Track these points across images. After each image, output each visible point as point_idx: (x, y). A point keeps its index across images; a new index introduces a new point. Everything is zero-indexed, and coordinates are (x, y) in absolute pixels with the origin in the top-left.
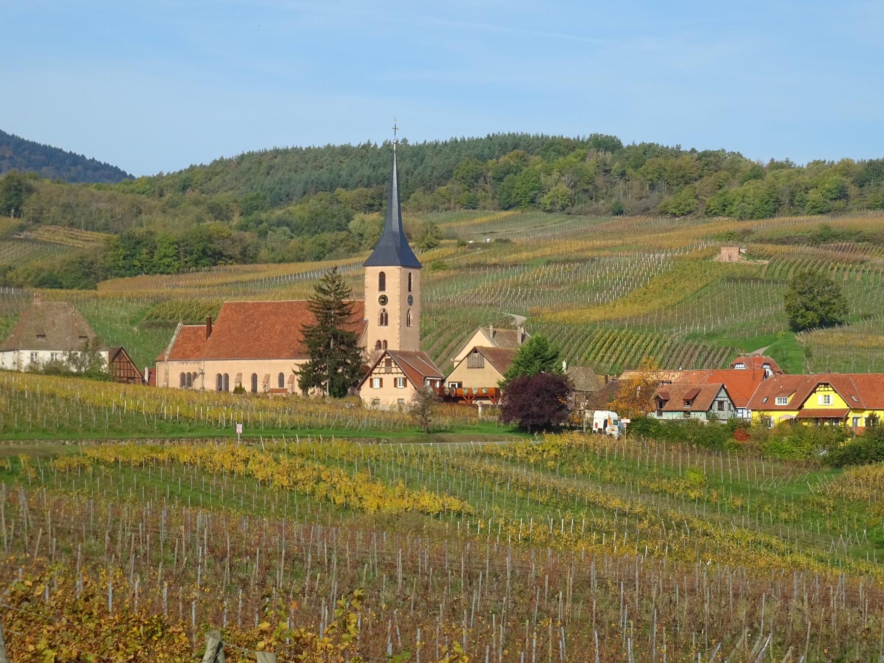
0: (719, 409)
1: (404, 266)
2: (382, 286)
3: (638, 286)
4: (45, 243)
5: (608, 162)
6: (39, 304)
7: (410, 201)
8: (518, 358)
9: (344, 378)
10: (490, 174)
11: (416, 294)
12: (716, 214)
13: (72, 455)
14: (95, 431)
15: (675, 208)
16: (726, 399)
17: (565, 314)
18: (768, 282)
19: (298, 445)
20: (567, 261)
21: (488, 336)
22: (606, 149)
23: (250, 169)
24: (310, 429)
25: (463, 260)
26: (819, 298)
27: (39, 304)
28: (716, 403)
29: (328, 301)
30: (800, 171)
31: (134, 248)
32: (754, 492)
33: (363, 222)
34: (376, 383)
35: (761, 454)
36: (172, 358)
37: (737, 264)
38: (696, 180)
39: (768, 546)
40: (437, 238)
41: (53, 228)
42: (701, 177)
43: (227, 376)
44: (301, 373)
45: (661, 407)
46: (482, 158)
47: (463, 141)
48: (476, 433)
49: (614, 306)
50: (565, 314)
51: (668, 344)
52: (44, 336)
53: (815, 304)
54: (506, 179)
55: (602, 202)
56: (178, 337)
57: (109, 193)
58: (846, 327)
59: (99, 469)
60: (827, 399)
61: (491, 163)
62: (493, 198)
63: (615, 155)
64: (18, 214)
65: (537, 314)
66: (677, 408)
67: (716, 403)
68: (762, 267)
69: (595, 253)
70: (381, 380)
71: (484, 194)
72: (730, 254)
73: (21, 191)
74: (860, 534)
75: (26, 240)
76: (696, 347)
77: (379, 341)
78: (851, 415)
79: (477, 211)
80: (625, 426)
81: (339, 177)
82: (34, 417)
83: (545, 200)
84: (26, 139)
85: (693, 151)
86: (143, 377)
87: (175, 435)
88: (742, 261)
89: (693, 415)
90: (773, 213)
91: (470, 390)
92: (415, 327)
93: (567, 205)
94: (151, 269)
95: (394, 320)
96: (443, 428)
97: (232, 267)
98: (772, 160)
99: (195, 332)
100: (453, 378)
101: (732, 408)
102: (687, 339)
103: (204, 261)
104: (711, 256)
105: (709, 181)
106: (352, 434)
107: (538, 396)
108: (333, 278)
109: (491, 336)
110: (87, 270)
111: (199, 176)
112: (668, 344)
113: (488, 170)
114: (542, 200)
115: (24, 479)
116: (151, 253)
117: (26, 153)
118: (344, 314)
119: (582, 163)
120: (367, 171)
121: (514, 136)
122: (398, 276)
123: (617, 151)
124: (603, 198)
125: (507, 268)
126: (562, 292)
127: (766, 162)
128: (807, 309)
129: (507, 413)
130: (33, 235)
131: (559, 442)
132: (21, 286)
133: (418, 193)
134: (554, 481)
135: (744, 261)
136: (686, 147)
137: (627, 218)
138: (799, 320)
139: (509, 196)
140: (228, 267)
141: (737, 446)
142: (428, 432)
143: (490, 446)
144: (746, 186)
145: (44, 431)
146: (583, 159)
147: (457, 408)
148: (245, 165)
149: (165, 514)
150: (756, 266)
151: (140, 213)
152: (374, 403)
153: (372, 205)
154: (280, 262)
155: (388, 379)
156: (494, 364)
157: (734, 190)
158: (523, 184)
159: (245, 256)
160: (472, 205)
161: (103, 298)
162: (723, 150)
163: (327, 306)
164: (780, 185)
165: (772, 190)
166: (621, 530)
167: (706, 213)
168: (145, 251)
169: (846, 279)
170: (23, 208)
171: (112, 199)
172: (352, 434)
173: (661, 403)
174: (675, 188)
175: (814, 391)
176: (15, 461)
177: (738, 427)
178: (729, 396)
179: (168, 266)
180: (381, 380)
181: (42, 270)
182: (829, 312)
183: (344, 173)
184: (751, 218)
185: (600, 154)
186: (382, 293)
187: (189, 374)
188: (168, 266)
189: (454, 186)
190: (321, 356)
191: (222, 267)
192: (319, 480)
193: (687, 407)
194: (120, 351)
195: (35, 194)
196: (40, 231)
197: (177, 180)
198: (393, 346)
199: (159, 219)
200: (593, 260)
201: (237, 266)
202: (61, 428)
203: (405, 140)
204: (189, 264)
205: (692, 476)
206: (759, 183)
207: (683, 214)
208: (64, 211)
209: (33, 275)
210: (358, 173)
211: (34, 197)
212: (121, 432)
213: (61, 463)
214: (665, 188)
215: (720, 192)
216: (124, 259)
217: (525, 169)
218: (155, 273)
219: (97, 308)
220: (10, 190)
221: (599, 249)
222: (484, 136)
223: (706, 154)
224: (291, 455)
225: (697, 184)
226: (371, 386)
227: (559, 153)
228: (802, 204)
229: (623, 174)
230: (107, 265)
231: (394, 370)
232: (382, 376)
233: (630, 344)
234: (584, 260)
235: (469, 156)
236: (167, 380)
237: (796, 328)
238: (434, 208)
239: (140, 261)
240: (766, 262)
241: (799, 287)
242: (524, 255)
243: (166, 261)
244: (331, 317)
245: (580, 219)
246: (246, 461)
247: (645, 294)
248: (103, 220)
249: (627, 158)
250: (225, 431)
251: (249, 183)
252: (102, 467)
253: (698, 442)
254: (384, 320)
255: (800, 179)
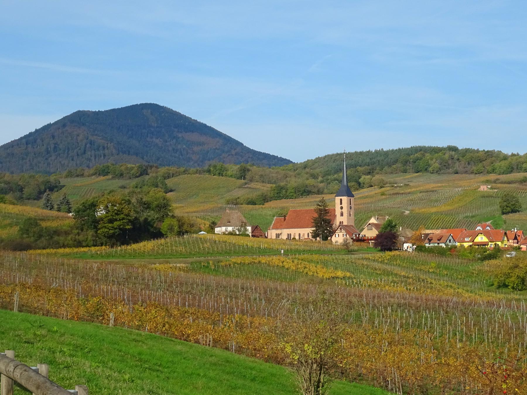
0: (449, 242)
1: (348, 196)
2: (341, 203)
3: (450, 200)
4: (253, 188)
5: (453, 155)
6: (228, 211)
7: (383, 170)
8: (383, 227)
9: (327, 234)
10: (411, 160)
11: (352, 206)
12: (491, 173)
13: (227, 261)
14: (237, 253)
15: (476, 171)
16: (452, 239)
17: (423, 210)
18: (496, 197)
19: (302, 256)
20: (427, 191)
21: (376, 219)
22: (453, 151)
23: (328, 160)
24: (310, 252)
25: (392, 192)
26: (511, 203)
27: (228, 211)
28: (448, 240)
29: (321, 209)
30: (521, 157)
31: (280, 190)
32: (452, 269)
33: (365, 179)
34: (337, 236)
35: (458, 257)
36: (273, 229)
37: (486, 191)
38: (484, 161)
39: (451, 287)
40: (384, 184)
41: (256, 183)
42: (486, 160)
43: (291, 234)
44: (312, 233)
45: (430, 242)
46: (409, 155)
47: (402, 149)
48: (366, 252)
49: (441, 207)
50: (423, 210)
51: (457, 220)
52: (230, 222)
53: (510, 205)
54: (417, 162)
55: (451, 169)
56: (275, 221)
57: (276, 171)
58: (521, 213)
59: (235, 265)
60: (482, 238)
61: (411, 156)
62: (412, 169)
63: (456, 153)
64: (244, 179)
65: (413, 210)
66: (435, 242)
67: (448, 240)
68: (494, 192)
69: (437, 189)
70: (339, 235)
71: (409, 167)
72: (484, 188)
73: (245, 170)
74: (483, 282)
75: (247, 188)
76: (467, 221)
77: (340, 222)
78: (490, 243)
79: (407, 174)
80: (414, 248)
81: (358, 163)
82: (218, 249)
83: (430, 169)
84: (257, 151)
85: (484, 150)
86: (265, 235)
87: (264, 254)
88: (488, 190)
89: (440, 245)
90: (511, 172)
91: (368, 237)
92: (352, 216)
93: (438, 171)
94: (287, 197)
95: (345, 214)
96: (353, 250)
97: (314, 196)
98: (512, 153)
99: (280, 220)
100: (362, 234)
101: (454, 242)
102: (464, 218)
103: (304, 194)
104: (478, 189)
105: (489, 161)
106: (331, 252)
107: (386, 239)
108: (323, 201)
109: (377, 219)
110: (264, 198)
111: (310, 164)
112: (457, 220)
113: (411, 159)
114: (429, 169)
115: (211, 269)
116: (286, 192)
117: (257, 155)
118: (327, 213)
119: (444, 156)
120: (368, 160)
121: (420, 147)
122: (346, 200)
123: (457, 151)
124: (451, 168)
125: (406, 194)
126: (424, 202)
127: (510, 154)
128: (507, 207)
129: (376, 245)
130: (250, 186)
131: (390, 254)
132: (242, 204)
133: (386, 168)
134: (385, 267)
135: (489, 190)
136: (481, 149)
137: (459, 175)
138: (504, 211)
139: (418, 168)
140: (313, 196)
141: (451, 254)
142: (349, 251)
143: (367, 256)
144: (501, 163)
145: (221, 253)
146: (444, 154)
147: (363, 243)
148: (326, 159)
149: (516, 298)
150: (492, 192)
151: (287, 177)
152: (336, 242)
153: (370, 172)
154: (331, 193)
155: (341, 234)
156: (376, 228)
157: (497, 164)
158: (423, 164)
159: (319, 192)
160: (405, 171)
161: (264, 208)
162: (494, 150)
163: (320, 210)
164: (513, 162)
165: (510, 164)
166: (402, 282)
167: (487, 173)
168: (284, 191)
169: (524, 196)
170: (246, 176)
171: (277, 173)
172: (331, 252)
173: (430, 241)
174: (476, 164)
175: (477, 236)
176: (209, 263)
177: (453, 248)
178: (453, 238)
179: (292, 196)
180: (339, 235)
181: (249, 198)
182: (514, 208)
183: (360, 161)
184: (503, 174)
185: (450, 152)
186: (341, 206)
187: (278, 234)
188: (292, 196)
189: (399, 165)
190: (319, 227)
191: (310, 196)
192: (305, 268)
193: (438, 242)
194: (257, 226)
195: (250, 172)
196: (252, 184)
197: (302, 165)
198: (345, 223)
199: (293, 179)
200: (436, 191)
201: (315, 195)
202: (226, 252)
203: (382, 149)
204: (299, 195)
205: (432, 264)
206: (506, 161)
207: (479, 173)
208: (261, 177)
209: (246, 200)
210: (365, 161)
211: (250, 172)
212: (246, 253)
213: (223, 264)
214: (473, 164)
215: (492, 165)
216: (277, 194)
217: (424, 158)
218: (288, 198)
219: (262, 211)
220: (242, 170)
221: (440, 187)
222: (410, 147)
223: (488, 151)
224: (299, 259)
225: (484, 162)
226: (335, 236)
227: (436, 152)
228: (521, 169)
229: (458, 159)
230: (271, 196)
231: (343, 231)
232: (339, 233)
233: (444, 220)
234: (433, 191)
235: (404, 154)
236: (271, 236)
237: (503, 213)
238: (392, 173)
239: (282, 194)
240: (496, 190)
241: (504, 199)
242: (413, 189)
243: (292, 194)
244: (322, 214)
245: (443, 176)
246: (283, 262)
247: (453, 202)
248: (274, 180)
249: (460, 154)
250: (277, 252)
251: (327, 166)
252: (236, 265)
253: (438, 253)
254: (342, 215)
255: (520, 160)
